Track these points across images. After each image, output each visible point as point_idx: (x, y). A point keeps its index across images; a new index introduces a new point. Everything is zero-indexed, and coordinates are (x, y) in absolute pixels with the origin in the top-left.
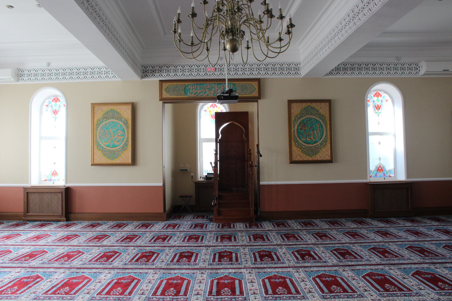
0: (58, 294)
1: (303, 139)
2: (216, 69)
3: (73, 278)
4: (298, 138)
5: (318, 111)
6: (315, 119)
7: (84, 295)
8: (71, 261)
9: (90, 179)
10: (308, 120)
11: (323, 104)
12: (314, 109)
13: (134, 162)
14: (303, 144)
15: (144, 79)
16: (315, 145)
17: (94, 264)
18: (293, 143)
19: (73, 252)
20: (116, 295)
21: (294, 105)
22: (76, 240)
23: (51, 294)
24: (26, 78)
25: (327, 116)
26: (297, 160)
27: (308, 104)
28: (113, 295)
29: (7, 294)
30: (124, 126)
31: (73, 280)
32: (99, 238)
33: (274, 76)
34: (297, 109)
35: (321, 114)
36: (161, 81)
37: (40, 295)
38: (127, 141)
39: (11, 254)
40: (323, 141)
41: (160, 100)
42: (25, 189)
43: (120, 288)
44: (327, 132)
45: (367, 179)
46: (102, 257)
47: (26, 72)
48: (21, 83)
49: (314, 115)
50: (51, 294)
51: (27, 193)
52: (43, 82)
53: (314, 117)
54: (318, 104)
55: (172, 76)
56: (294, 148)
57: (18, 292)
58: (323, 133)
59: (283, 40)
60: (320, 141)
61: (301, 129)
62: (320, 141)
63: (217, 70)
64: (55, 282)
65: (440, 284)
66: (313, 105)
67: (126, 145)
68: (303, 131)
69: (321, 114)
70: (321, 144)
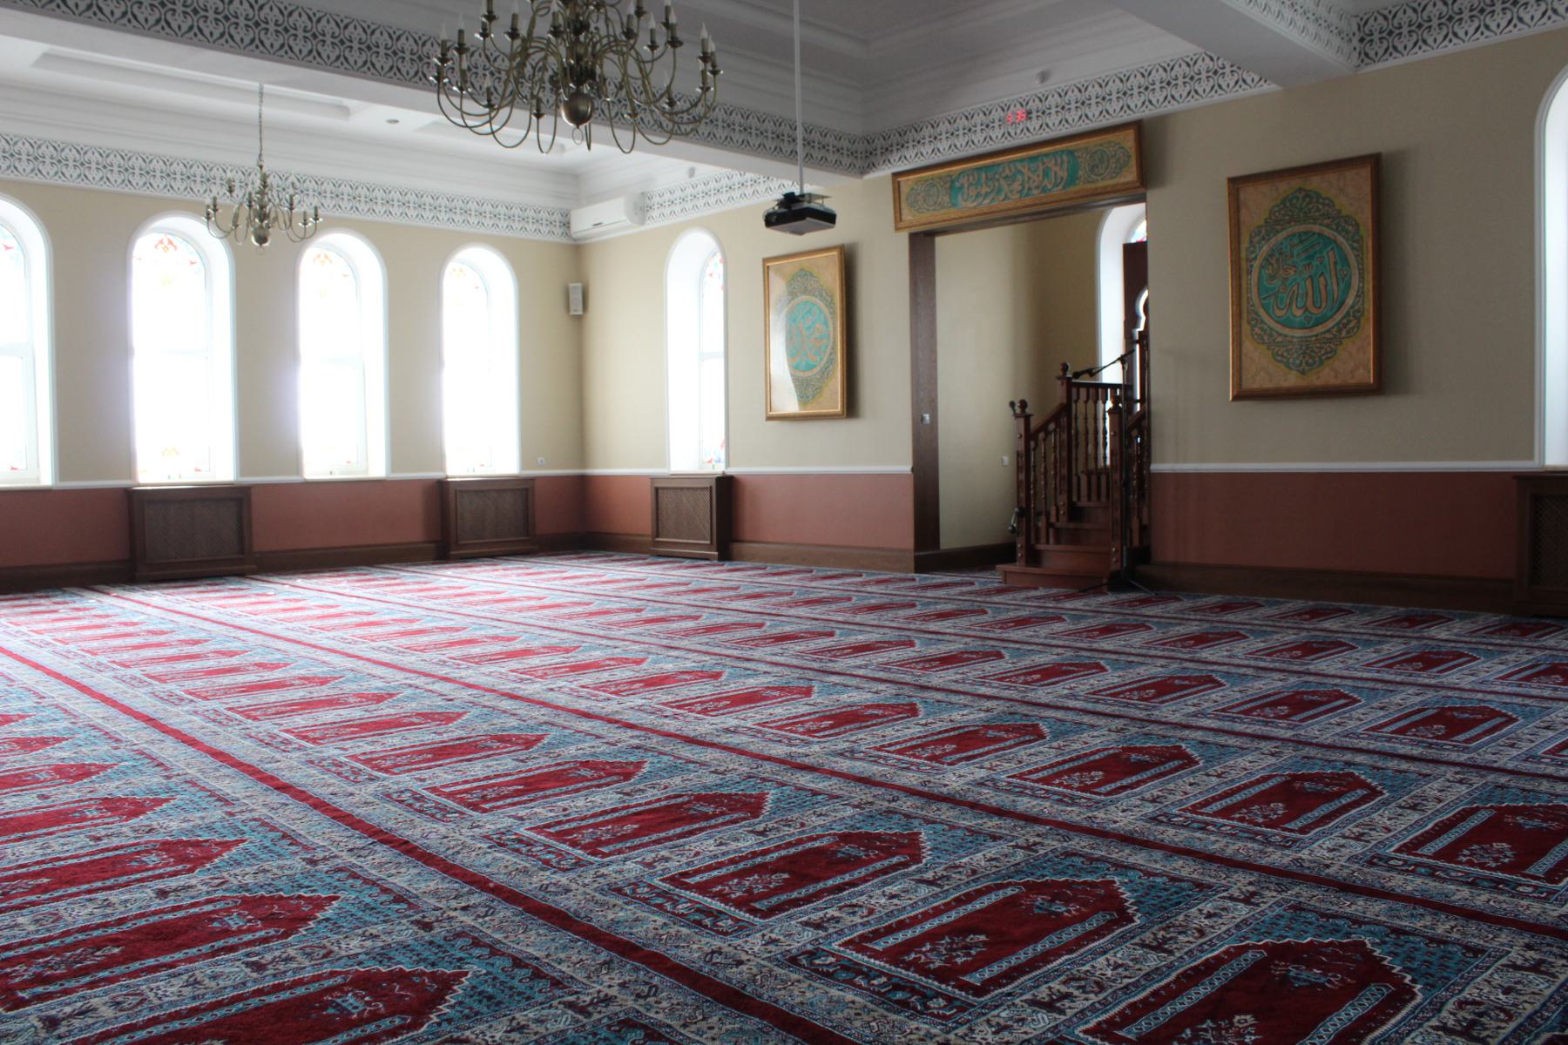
0: (1242, 820)
1: (1279, 313)
2: (1029, 113)
3: (1304, 778)
4: (1261, 312)
5: (1331, 204)
6: (1320, 235)
7: (1343, 841)
8: (1302, 720)
9: (765, 459)
10: (1296, 240)
11: (1349, 174)
12: (1318, 196)
13: (851, 407)
14: (1278, 328)
15: (867, 177)
16: (1319, 329)
17: (1389, 740)
18: (1246, 327)
19: (1314, 693)
20: (1482, 866)
21: (1248, 194)
22: (1338, 658)
23: (1215, 814)
24: (655, 213)
25: (1365, 217)
26: (1255, 386)
27: (1296, 183)
28: (1470, 863)
29: (1066, 787)
30: (826, 311)
31: (1307, 785)
32: (1429, 660)
33: (1192, 103)
34: (1260, 203)
35: (1344, 213)
36: (896, 175)
37: (1175, 811)
38: (834, 348)
39: (1100, 676)
40: (1348, 314)
41: (897, 229)
42: (653, 479)
43: (1505, 845)
44: (1362, 277)
45: (1531, 457)
46: (1427, 722)
47: (656, 199)
48: (649, 225)
49: (1315, 221)
50: (1215, 814)
51: (657, 489)
52: (465, 228)
53: (1317, 228)
54: (1332, 177)
55: (945, 150)
56: (1248, 345)
57: (1103, 789)
58: (1349, 286)
59: (681, 44)
60: (1338, 317)
61: (1272, 278)
62: (1338, 317)
63: (1034, 115)
64: (1237, 776)
65: (629, 828)
66: (1315, 183)
67: (831, 361)
68: (1277, 283)
69: (1344, 213)
70: (1342, 326)
